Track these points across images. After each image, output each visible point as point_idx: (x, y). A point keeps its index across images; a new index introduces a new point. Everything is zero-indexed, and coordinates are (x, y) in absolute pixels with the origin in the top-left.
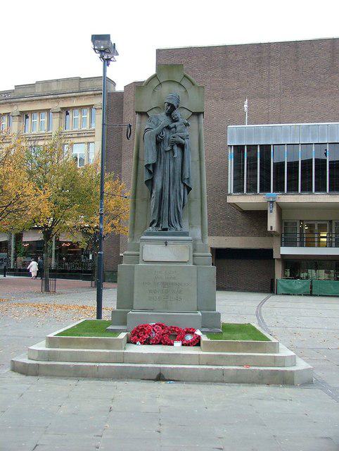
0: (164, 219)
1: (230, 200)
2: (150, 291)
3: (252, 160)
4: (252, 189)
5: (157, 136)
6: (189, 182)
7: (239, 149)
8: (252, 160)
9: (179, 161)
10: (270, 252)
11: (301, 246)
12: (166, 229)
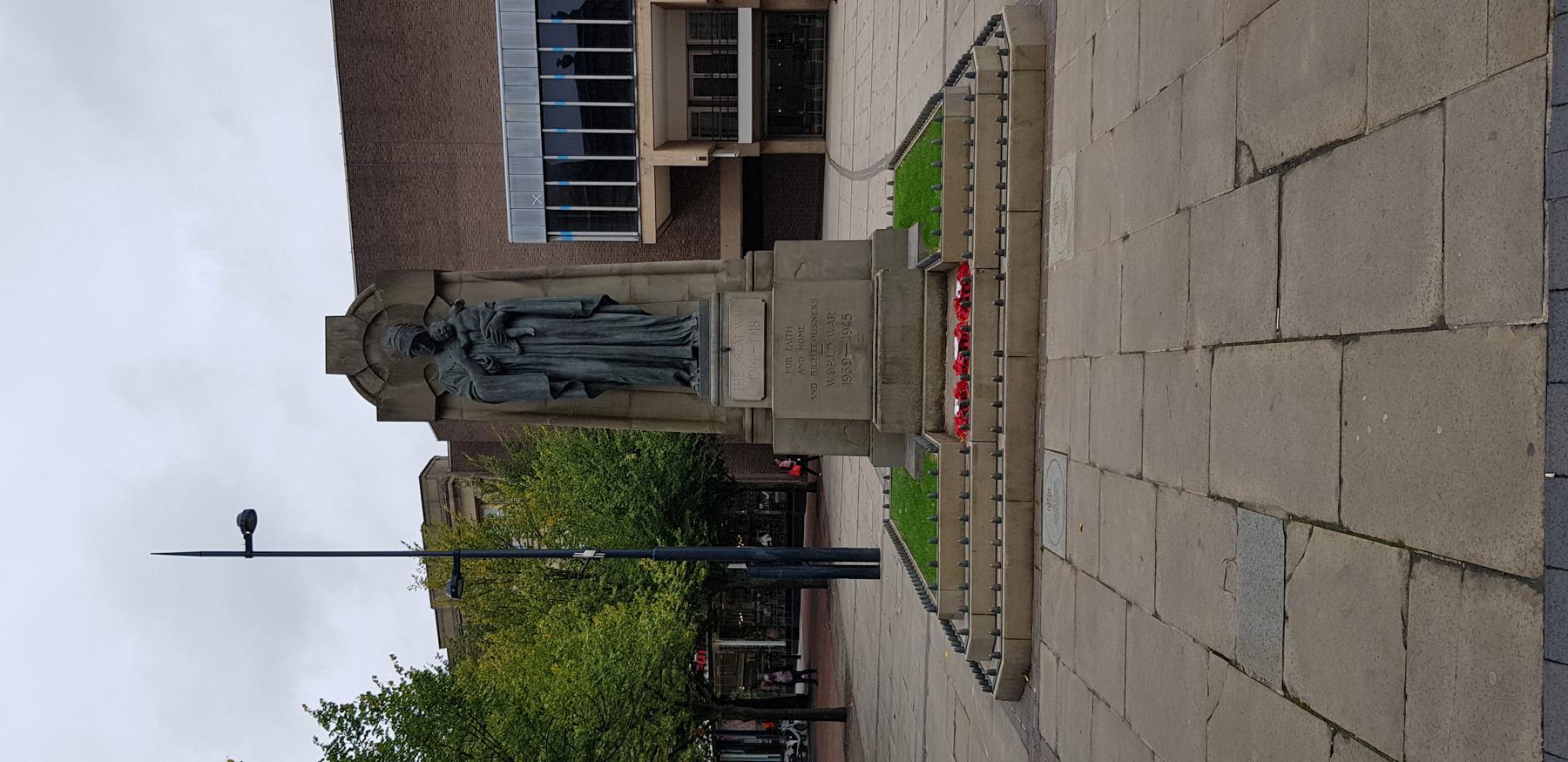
0: (678, 355)
1: (650, 237)
2: (831, 382)
3: (578, 196)
4: (631, 196)
5: (487, 373)
6: (591, 302)
7: (555, 222)
8: (578, 196)
9: (546, 323)
10: (747, 161)
11: (736, 104)
12: (695, 350)
